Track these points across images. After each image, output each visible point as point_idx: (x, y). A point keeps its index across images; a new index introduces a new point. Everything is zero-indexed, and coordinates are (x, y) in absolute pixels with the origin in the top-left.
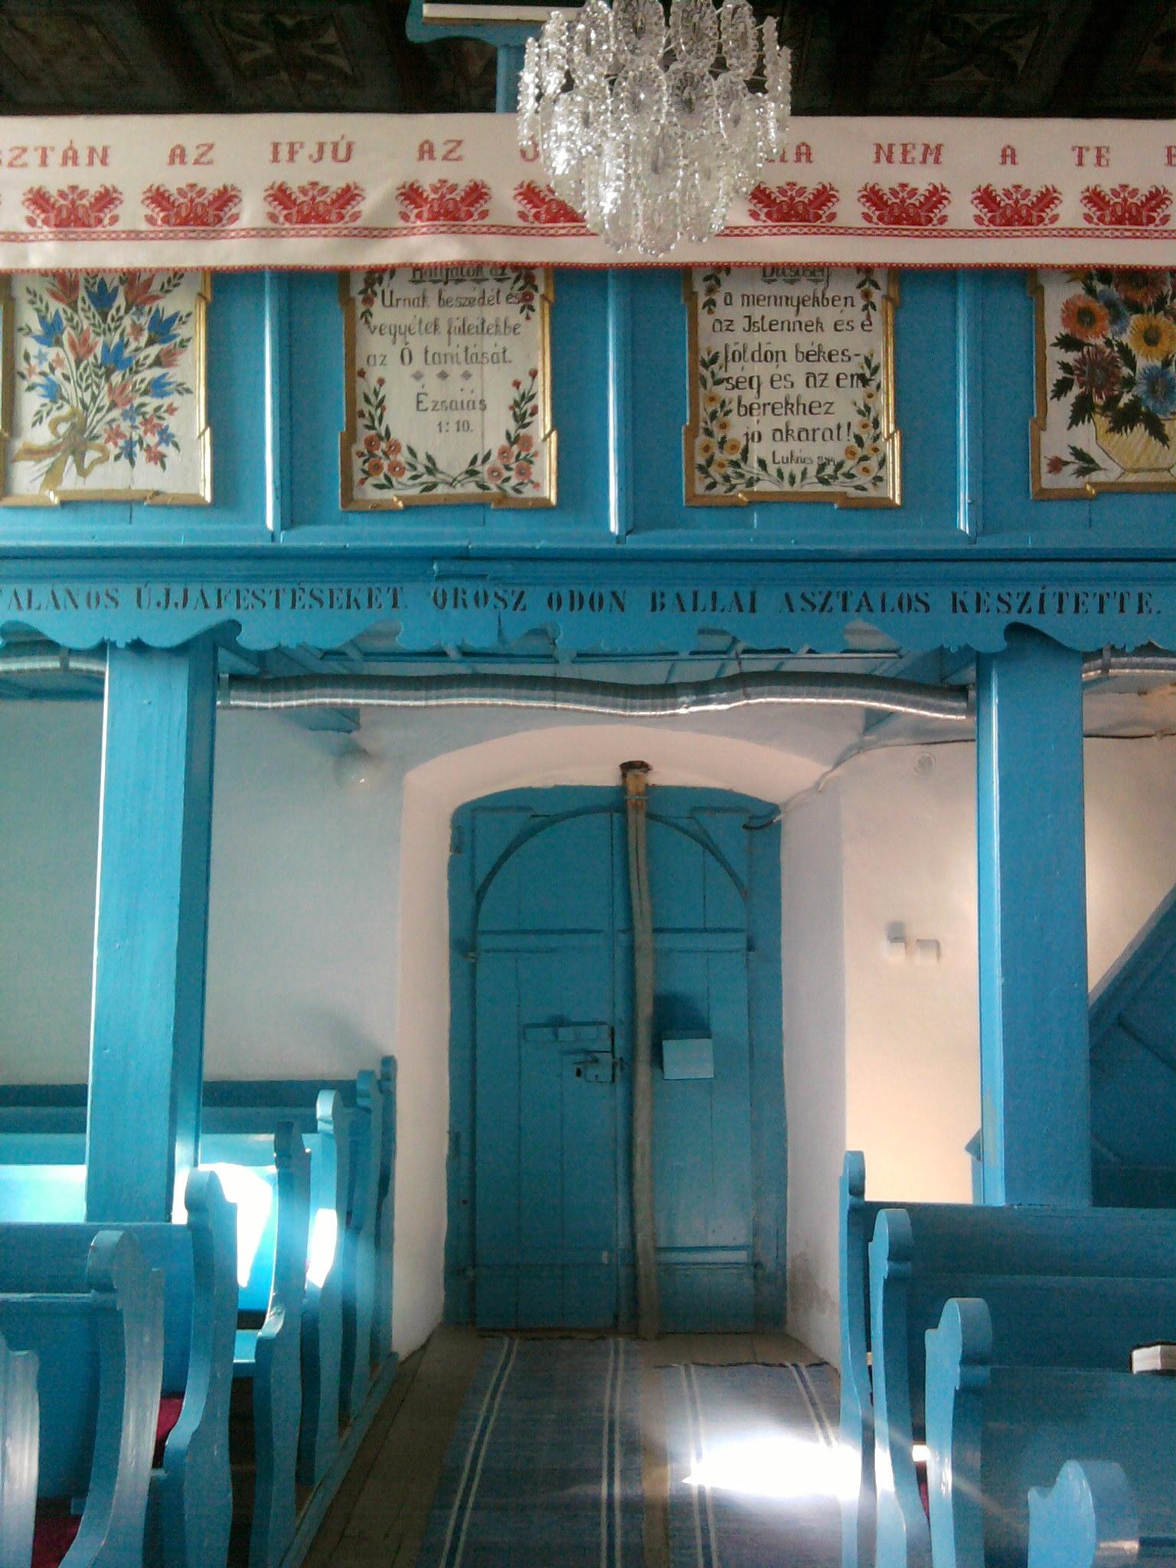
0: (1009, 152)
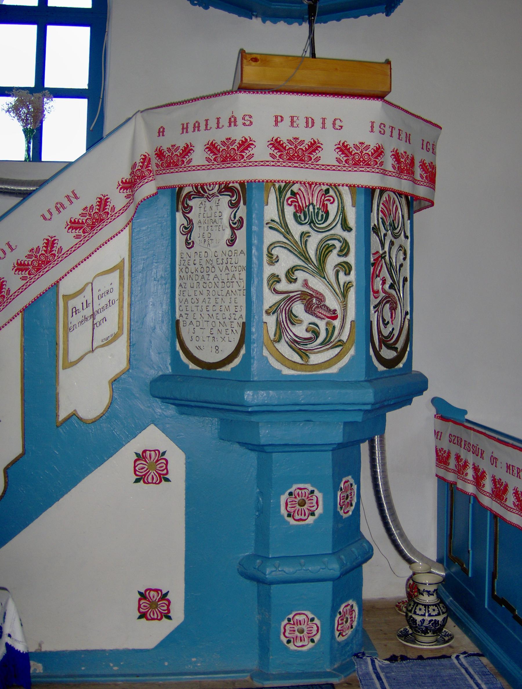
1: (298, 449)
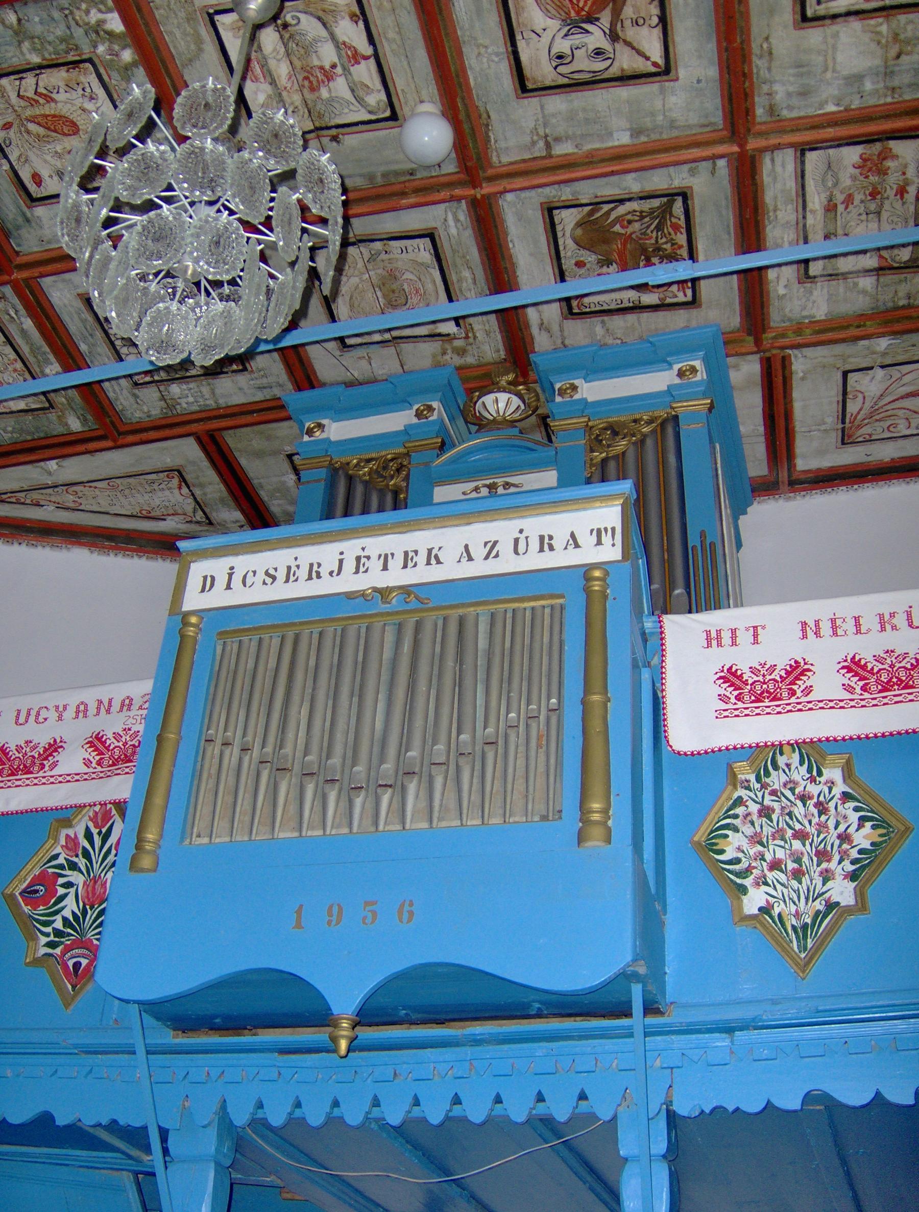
0: (82, 708)
1: (167, 432)
